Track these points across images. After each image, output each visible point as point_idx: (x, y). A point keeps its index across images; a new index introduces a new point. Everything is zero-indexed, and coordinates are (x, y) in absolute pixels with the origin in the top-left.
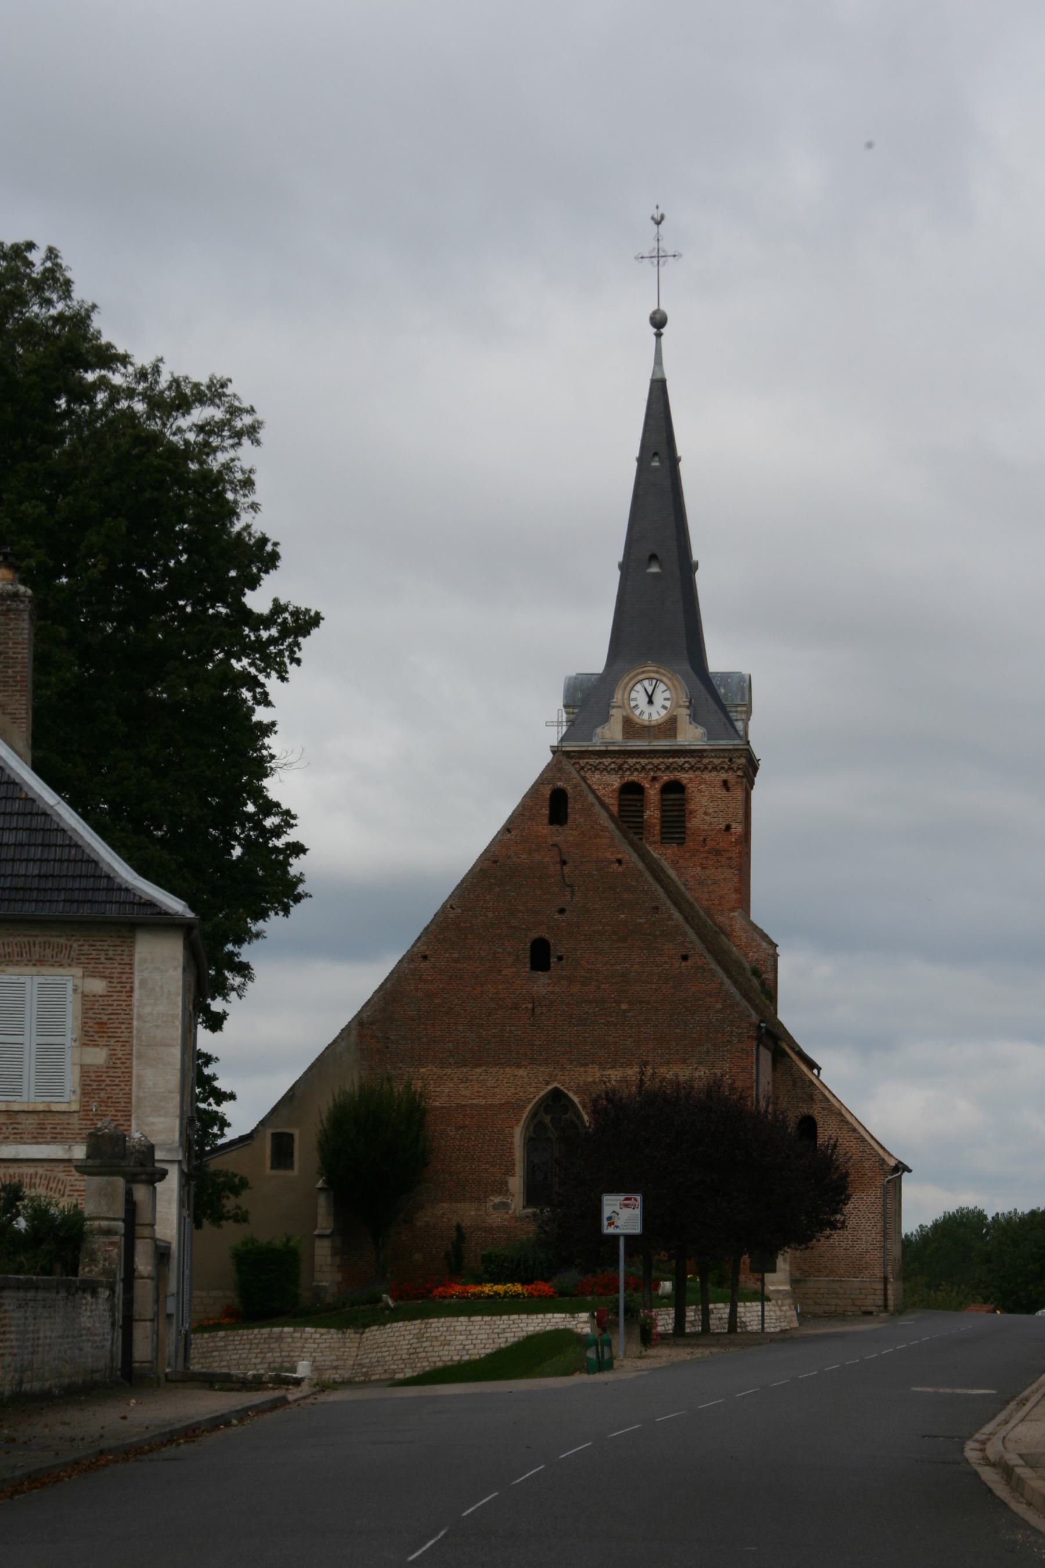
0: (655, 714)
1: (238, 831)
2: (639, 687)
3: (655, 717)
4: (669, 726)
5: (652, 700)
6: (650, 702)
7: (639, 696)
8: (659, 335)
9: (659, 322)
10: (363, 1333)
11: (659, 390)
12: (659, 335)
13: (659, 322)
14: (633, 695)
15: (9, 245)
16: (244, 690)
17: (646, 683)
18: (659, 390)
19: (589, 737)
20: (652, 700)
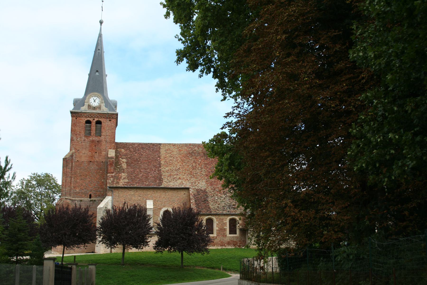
0: (95, 104)
1: (372, 124)
2: (92, 98)
3: (96, 105)
4: (99, 107)
5: (95, 101)
6: (95, 101)
7: (92, 100)
8: (101, 25)
9: (101, 22)
10: (226, 188)
11: (100, 36)
12: (101, 25)
13: (101, 22)
14: (90, 100)
15: (230, 104)
16: (303, 166)
17: (94, 97)
18: (100, 36)
19: (79, 109)
20: (95, 101)
